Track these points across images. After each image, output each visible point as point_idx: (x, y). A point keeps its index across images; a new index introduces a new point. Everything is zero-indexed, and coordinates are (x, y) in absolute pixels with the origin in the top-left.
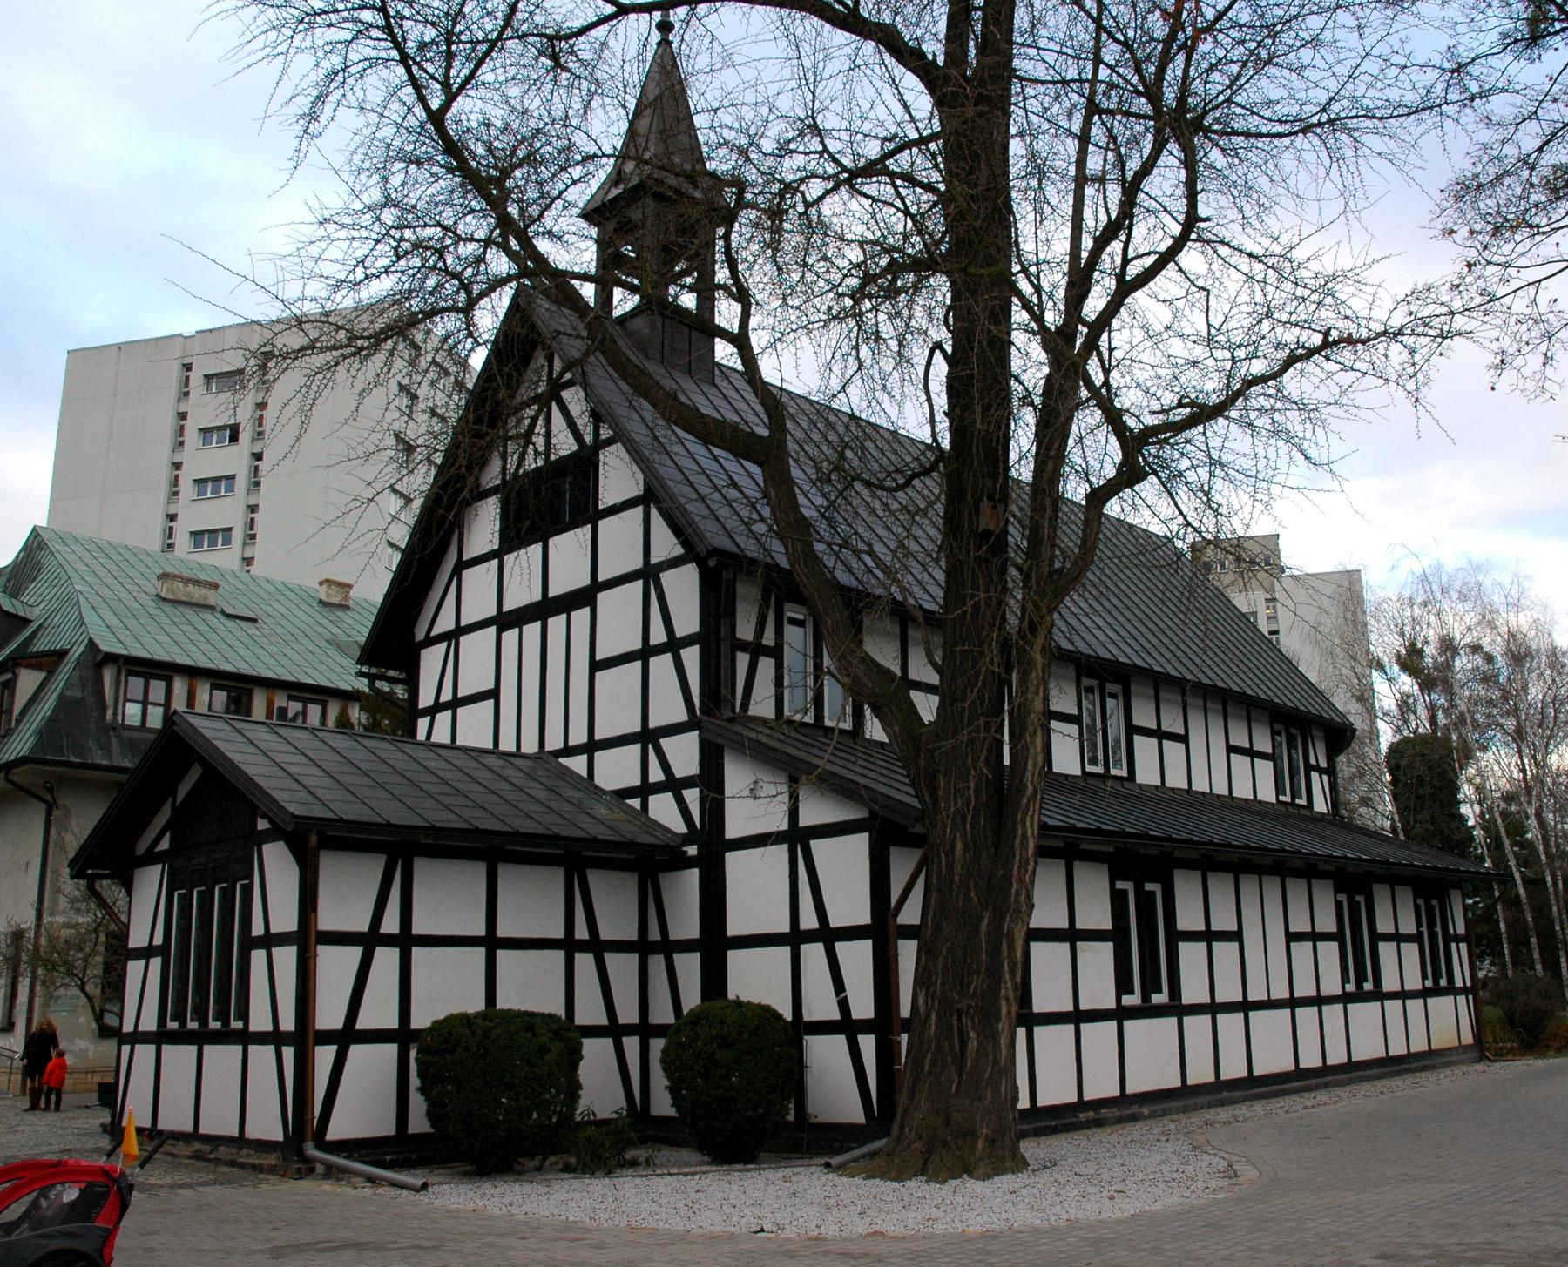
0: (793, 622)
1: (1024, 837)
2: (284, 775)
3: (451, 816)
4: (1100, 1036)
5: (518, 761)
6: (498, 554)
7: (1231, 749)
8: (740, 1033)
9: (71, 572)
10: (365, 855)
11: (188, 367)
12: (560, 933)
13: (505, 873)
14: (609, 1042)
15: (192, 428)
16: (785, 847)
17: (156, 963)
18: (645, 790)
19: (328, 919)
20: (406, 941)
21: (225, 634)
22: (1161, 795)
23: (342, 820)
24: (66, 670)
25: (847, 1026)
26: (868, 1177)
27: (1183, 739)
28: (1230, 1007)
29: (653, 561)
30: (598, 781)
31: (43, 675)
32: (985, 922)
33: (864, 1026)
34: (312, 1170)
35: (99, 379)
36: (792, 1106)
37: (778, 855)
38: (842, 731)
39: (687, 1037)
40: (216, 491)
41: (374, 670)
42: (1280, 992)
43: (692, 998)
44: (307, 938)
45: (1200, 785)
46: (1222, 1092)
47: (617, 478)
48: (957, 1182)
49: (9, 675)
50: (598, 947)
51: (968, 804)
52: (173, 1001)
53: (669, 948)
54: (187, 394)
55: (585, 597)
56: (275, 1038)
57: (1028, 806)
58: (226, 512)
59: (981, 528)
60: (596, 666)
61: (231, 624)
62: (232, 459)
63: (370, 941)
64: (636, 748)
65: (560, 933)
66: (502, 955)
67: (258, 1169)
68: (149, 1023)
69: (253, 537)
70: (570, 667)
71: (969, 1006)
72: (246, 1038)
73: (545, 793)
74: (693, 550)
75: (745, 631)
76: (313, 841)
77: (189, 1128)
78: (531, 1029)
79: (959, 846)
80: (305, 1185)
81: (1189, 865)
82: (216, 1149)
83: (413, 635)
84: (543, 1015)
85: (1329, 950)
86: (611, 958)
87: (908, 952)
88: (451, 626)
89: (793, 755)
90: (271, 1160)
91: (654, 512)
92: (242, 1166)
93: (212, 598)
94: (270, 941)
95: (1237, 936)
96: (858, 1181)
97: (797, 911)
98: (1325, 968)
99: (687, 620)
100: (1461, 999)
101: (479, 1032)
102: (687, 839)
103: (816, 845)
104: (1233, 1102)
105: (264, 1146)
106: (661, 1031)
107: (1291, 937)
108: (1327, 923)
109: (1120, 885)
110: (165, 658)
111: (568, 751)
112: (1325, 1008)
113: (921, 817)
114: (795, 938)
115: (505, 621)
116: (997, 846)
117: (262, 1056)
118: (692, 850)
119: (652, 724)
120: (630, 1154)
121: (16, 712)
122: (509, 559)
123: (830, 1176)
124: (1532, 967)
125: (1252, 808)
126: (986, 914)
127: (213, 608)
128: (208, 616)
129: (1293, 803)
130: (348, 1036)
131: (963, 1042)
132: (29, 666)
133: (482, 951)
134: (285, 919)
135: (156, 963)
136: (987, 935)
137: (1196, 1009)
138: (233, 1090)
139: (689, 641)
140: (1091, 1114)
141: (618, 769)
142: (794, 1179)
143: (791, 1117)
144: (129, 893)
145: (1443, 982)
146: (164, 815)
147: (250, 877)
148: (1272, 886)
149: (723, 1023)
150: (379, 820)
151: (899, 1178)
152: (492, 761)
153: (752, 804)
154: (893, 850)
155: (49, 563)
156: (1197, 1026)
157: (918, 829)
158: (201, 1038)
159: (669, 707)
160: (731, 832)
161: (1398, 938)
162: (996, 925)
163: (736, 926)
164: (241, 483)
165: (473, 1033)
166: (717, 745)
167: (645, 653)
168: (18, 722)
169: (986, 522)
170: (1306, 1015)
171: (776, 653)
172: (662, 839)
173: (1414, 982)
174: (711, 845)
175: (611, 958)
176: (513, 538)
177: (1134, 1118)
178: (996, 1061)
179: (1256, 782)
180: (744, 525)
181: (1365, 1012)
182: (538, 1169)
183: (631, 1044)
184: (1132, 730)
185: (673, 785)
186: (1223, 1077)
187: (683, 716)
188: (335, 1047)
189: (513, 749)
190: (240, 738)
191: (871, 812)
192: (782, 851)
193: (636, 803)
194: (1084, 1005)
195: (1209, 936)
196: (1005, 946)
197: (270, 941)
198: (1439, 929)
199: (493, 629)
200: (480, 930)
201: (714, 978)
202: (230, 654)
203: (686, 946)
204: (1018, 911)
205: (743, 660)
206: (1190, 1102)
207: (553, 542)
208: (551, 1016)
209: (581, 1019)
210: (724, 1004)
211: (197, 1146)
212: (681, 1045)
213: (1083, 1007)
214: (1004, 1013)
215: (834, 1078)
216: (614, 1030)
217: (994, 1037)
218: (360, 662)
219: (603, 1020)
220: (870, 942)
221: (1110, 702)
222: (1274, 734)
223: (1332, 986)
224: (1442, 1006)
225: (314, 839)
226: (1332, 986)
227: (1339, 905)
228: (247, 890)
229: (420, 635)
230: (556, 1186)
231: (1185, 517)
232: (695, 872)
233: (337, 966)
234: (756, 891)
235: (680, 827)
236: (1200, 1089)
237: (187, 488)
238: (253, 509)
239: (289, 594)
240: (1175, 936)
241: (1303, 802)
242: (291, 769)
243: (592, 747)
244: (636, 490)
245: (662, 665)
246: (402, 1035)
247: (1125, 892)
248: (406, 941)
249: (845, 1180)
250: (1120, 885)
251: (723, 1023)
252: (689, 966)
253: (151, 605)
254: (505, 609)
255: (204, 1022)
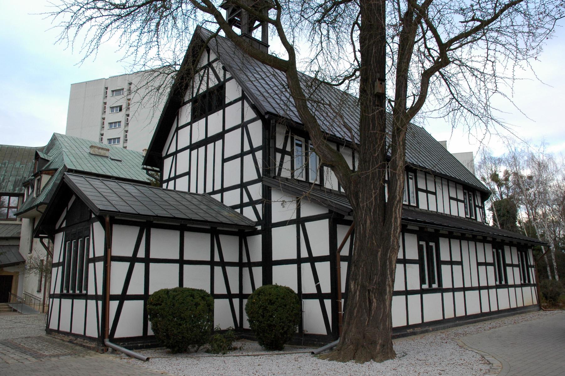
0: (297, 145)
1: (396, 218)
2: (101, 196)
3: (165, 212)
4: (414, 299)
5: (196, 196)
6: (190, 124)
7: (451, 198)
8: (277, 299)
9: (62, 145)
10: (131, 227)
11: (107, 88)
12: (208, 259)
13: (186, 234)
14: (227, 301)
15: (108, 106)
16: (295, 225)
17: (60, 268)
18: (242, 205)
19: (116, 251)
20: (147, 261)
21: (110, 165)
22: (427, 213)
23: (119, 212)
24: (57, 174)
25: (319, 296)
26: (330, 360)
27: (435, 194)
28: (459, 290)
29: (245, 120)
30: (224, 203)
31: (50, 177)
32: (379, 253)
33: (327, 296)
34: (108, 350)
35: (79, 91)
36: (298, 328)
37: (293, 228)
38: (316, 184)
39: (256, 300)
40: (115, 126)
41: (149, 167)
42: (475, 284)
43: (259, 284)
44: (108, 259)
45: (440, 210)
46: (458, 321)
47: (232, 91)
48: (368, 363)
49: (39, 177)
50: (223, 264)
51: (372, 204)
52: (65, 283)
53: (250, 265)
54: (106, 97)
55: (220, 136)
56: (96, 297)
57: (397, 205)
58: (118, 133)
59: (375, 93)
60: (224, 161)
61: (113, 162)
62: (120, 117)
63: (133, 260)
64: (239, 190)
65: (208, 259)
66: (186, 267)
67: (89, 348)
68: (58, 291)
69: (127, 140)
70: (217, 164)
71: (373, 288)
72: (87, 297)
73: (206, 207)
74: (260, 114)
75: (279, 145)
76: (112, 220)
77: (69, 331)
78: (192, 296)
79: (368, 222)
80: (104, 356)
81: (444, 236)
82: (76, 339)
83: (162, 155)
84: (198, 290)
85: (491, 269)
86: (228, 269)
87: (344, 266)
88: (175, 150)
89: (298, 190)
90: (93, 345)
91: (245, 101)
92: (84, 346)
93: (107, 154)
94: (95, 260)
95: (460, 263)
96: (326, 361)
97: (301, 250)
98: (489, 276)
99: (258, 141)
100: (533, 288)
101: (171, 297)
102: (257, 224)
103: (307, 224)
104: (461, 325)
105: (91, 339)
106: (246, 296)
107: (479, 264)
108: (490, 260)
109: (421, 243)
110: (88, 170)
111: (214, 192)
112: (490, 290)
113: (350, 213)
114: (299, 261)
115: (192, 147)
116: (384, 221)
117: (92, 303)
118: (259, 228)
119: (244, 181)
120: (235, 344)
121: (41, 189)
122: (195, 125)
123: (314, 358)
124: (548, 277)
125: (457, 219)
126: (380, 250)
127: (107, 157)
128: (105, 159)
129: (470, 218)
130: (123, 297)
131: (370, 303)
132: (46, 174)
133: (178, 265)
134: (100, 252)
135: (60, 268)
136: (381, 259)
137: (447, 290)
138: (81, 317)
139: (258, 149)
140: (412, 330)
141: (232, 198)
142: (300, 360)
143: (297, 332)
144: (53, 243)
145: (503, 283)
146: (64, 214)
147: (89, 236)
148: (472, 244)
149: (270, 294)
150: (135, 212)
151: (344, 361)
152: (187, 196)
153: (283, 209)
154: (338, 226)
155: (57, 143)
156: (448, 296)
157: (347, 218)
158: (73, 297)
159: (251, 174)
160: (274, 220)
161: (512, 265)
162: (385, 254)
163: (276, 256)
164: (123, 124)
165: (169, 297)
166: (269, 187)
167: (242, 155)
168: (42, 192)
169: (378, 90)
170: (484, 292)
171: (291, 154)
172: (247, 223)
173: (518, 282)
174: (266, 225)
175: (228, 269)
176: (195, 118)
177: (427, 331)
178: (384, 312)
179: (458, 210)
180: (281, 103)
181: (502, 292)
182: (196, 352)
183: (236, 301)
184: (418, 190)
185: (252, 203)
186: (457, 316)
187: (256, 177)
188: (118, 301)
189: (195, 192)
190: (88, 183)
191: (329, 210)
192: (293, 227)
193: (238, 211)
194: (409, 288)
195: (451, 263)
196: (388, 263)
197: (95, 260)
198: (525, 263)
199: (188, 150)
200: (177, 257)
201: (267, 277)
202: (111, 170)
203: (257, 264)
204: (393, 248)
205: (279, 156)
206: (446, 325)
207: (209, 117)
208: (202, 291)
209: (305, 291)
210: (271, 286)
211: (71, 337)
212: (254, 303)
213: (408, 289)
214: (388, 291)
215: (314, 317)
216: (229, 296)
217: (384, 301)
218: (143, 164)
219: (225, 292)
220: (329, 262)
221: (410, 181)
222: (465, 194)
223: (492, 283)
224: (527, 290)
225: (108, 219)
226: (492, 283)
227: (493, 252)
228: (89, 240)
229: (164, 154)
230: (202, 360)
231: (453, 95)
232: (260, 236)
233: (119, 270)
234: (284, 243)
235: (255, 219)
236: (449, 320)
237: (106, 126)
238: (127, 131)
239: (134, 154)
240: (440, 263)
241: (474, 218)
242: (104, 194)
243: (223, 190)
244: (239, 95)
245: (248, 159)
246: (145, 297)
247: (422, 245)
248: (147, 261)
249: (321, 361)
250: (421, 243)
251: (270, 294)
252: (258, 272)
253: (87, 155)
254: (193, 143)
255: (74, 291)
